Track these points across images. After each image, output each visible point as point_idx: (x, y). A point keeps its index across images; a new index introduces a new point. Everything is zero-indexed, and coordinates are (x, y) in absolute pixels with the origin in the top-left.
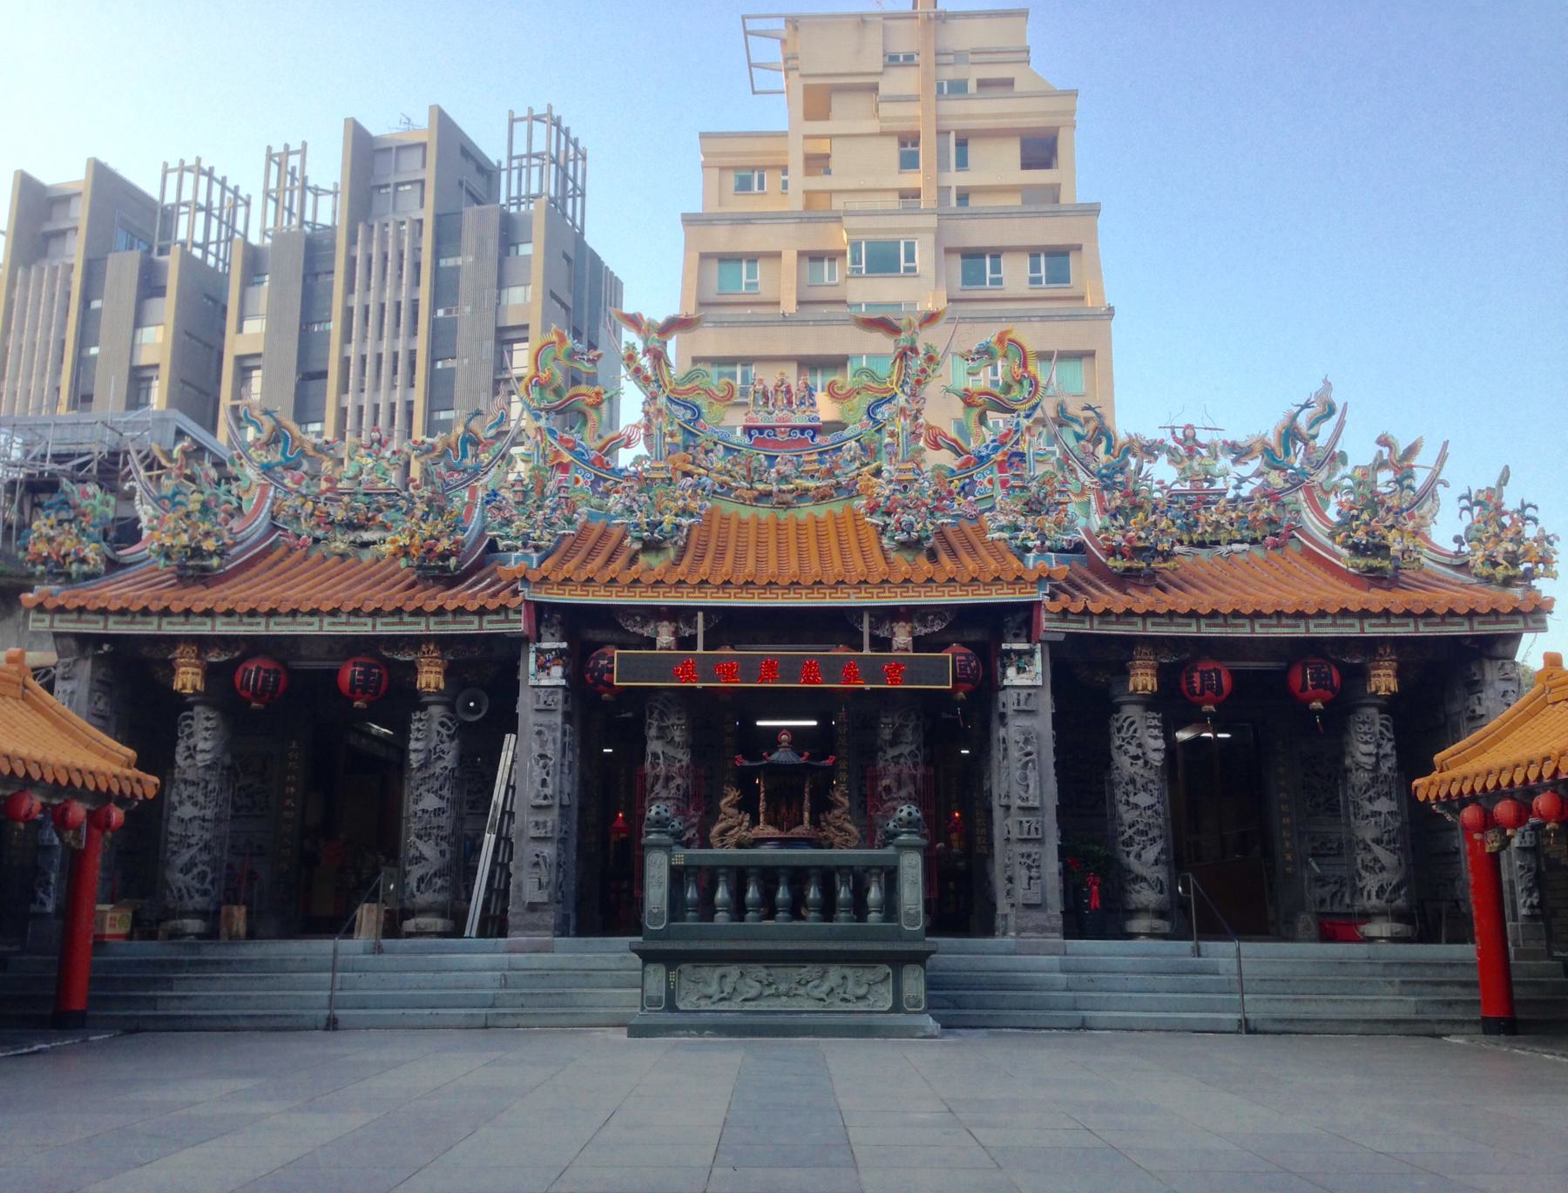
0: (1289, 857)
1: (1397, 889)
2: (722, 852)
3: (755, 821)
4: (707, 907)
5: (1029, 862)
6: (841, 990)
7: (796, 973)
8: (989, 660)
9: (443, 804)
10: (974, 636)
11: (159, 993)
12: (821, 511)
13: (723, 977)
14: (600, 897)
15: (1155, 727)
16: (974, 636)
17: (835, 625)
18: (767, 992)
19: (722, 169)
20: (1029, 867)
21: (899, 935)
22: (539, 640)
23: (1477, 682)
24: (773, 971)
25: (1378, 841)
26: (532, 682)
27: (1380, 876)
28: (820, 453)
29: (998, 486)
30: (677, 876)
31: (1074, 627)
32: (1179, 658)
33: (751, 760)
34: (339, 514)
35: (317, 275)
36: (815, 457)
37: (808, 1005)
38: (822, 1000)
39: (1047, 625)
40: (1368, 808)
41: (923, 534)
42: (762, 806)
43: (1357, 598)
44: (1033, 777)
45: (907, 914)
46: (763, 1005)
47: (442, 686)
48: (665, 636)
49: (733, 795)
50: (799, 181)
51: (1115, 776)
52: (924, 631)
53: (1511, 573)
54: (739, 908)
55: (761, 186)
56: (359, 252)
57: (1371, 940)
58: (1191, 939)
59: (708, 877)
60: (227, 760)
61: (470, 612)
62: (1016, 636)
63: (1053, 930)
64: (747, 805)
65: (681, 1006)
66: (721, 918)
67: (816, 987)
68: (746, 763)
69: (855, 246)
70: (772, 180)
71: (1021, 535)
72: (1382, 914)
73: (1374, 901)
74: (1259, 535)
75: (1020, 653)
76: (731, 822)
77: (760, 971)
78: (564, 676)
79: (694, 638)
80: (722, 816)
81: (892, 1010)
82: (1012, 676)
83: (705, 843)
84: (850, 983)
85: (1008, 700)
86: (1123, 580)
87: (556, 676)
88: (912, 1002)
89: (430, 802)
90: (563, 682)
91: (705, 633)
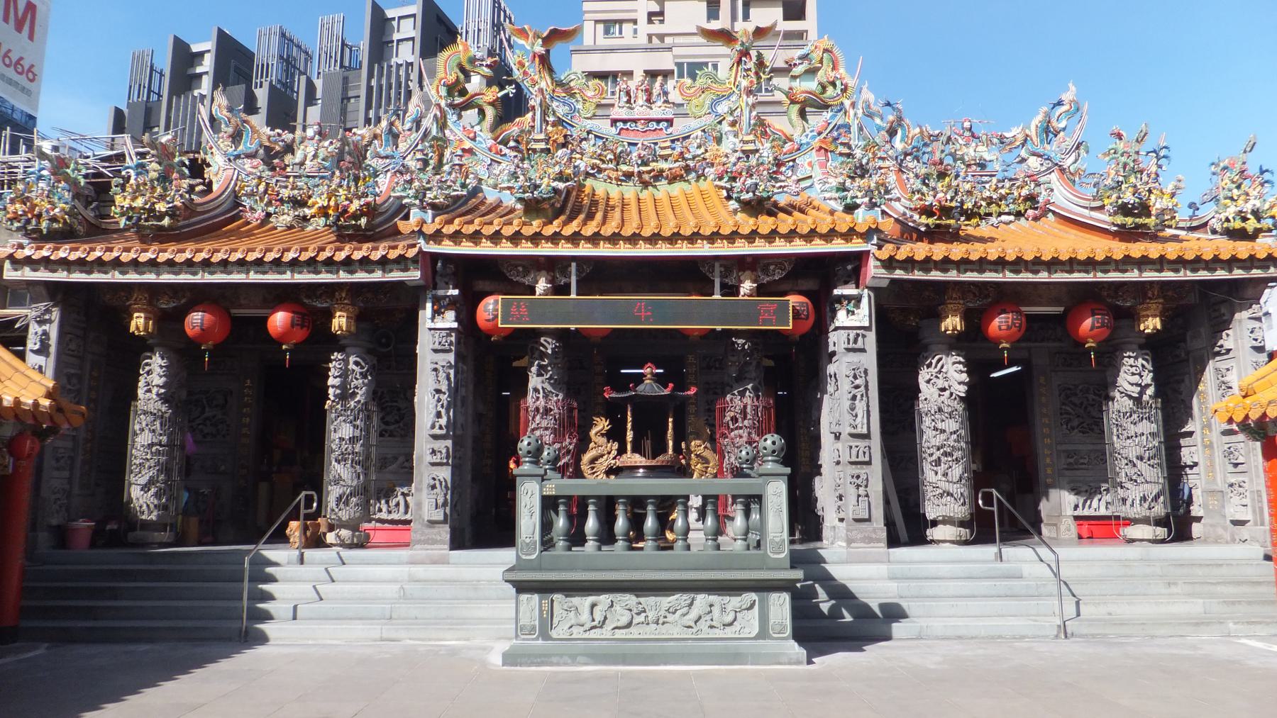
0: (1049, 471)
1: (1156, 498)
2: (595, 482)
3: (622, 451)
4: (576, 538)
5: (859, 482)
6: (708, 617)
7: (666, 601)
8: (824, 307)
9: (357, 433)
10: (810, 285)
11: (100, 603)
12: (677, 189)
13: (593, 606)
14: (482, 518)
15: (960, 363)
16: (810, 285)
17: (689, 275)
18: (638, 619)
19: (597, 22)
20: (858, 486)
21: (764, 564)
22: (435, 288)
23: (1225, 321)
24: (642, 600)
25: (1141, 458)
26: (430, 324)
27: (1141, 487)
28: (673, 141)
29: (816, 167)
30: (549, 504)
31: (899, 274)
32: (983, 301)
33: (618, 391)
34: (285, 193)
35: (349, 99)
36: (668, 144)
37: (675, 631)
38: (690, 627)
39: (873, 270)
40: (1132, 430)
41: (765, 195)
42: (630, 436)
43: (1119, 249)
44: (860, 406)
45: (772, 541)
46: (634, 632)
47: (353, 329)
48: (542, 285)
49: (602, 424)
50: (644, 28)
51: (922, 406)
52: (766, 280)
53: (1259, 226)
54: (606, 536)
55: (621, 32)
56: (374, 83)
57: (1132, 541)
58: (992, 541)
59: (577, 509)
60: (183, 394)
61: (376, 262)
62: (846, 283)
63: (878, 541)
64: (615, 434)
65: (554, 634)
66: (591, 545)
67: (684, 615)
68: (614, 395)
69: (680, 65)
70: (627, 28)
71: (850, 194)
72: (1145, 521)
73: (1137, 507)
74: (1022, 208)
75: (849, 298)
76: (600, 450)
77: (630, 599)
78: (457, 319)
79: (568, 286)
80: (592, 445)
81: (757, 638)
82: (842, 318)
83: (578, 474)
84: (716, 610)
85: (836, 340)
86: (932, 235)
87: (449, 320)
88: (778, 628)
89: (346, 431)
90: (455, 325)
91: (578, 282)
